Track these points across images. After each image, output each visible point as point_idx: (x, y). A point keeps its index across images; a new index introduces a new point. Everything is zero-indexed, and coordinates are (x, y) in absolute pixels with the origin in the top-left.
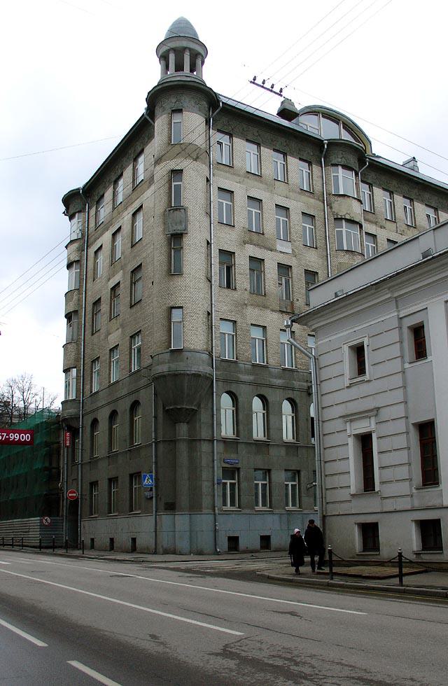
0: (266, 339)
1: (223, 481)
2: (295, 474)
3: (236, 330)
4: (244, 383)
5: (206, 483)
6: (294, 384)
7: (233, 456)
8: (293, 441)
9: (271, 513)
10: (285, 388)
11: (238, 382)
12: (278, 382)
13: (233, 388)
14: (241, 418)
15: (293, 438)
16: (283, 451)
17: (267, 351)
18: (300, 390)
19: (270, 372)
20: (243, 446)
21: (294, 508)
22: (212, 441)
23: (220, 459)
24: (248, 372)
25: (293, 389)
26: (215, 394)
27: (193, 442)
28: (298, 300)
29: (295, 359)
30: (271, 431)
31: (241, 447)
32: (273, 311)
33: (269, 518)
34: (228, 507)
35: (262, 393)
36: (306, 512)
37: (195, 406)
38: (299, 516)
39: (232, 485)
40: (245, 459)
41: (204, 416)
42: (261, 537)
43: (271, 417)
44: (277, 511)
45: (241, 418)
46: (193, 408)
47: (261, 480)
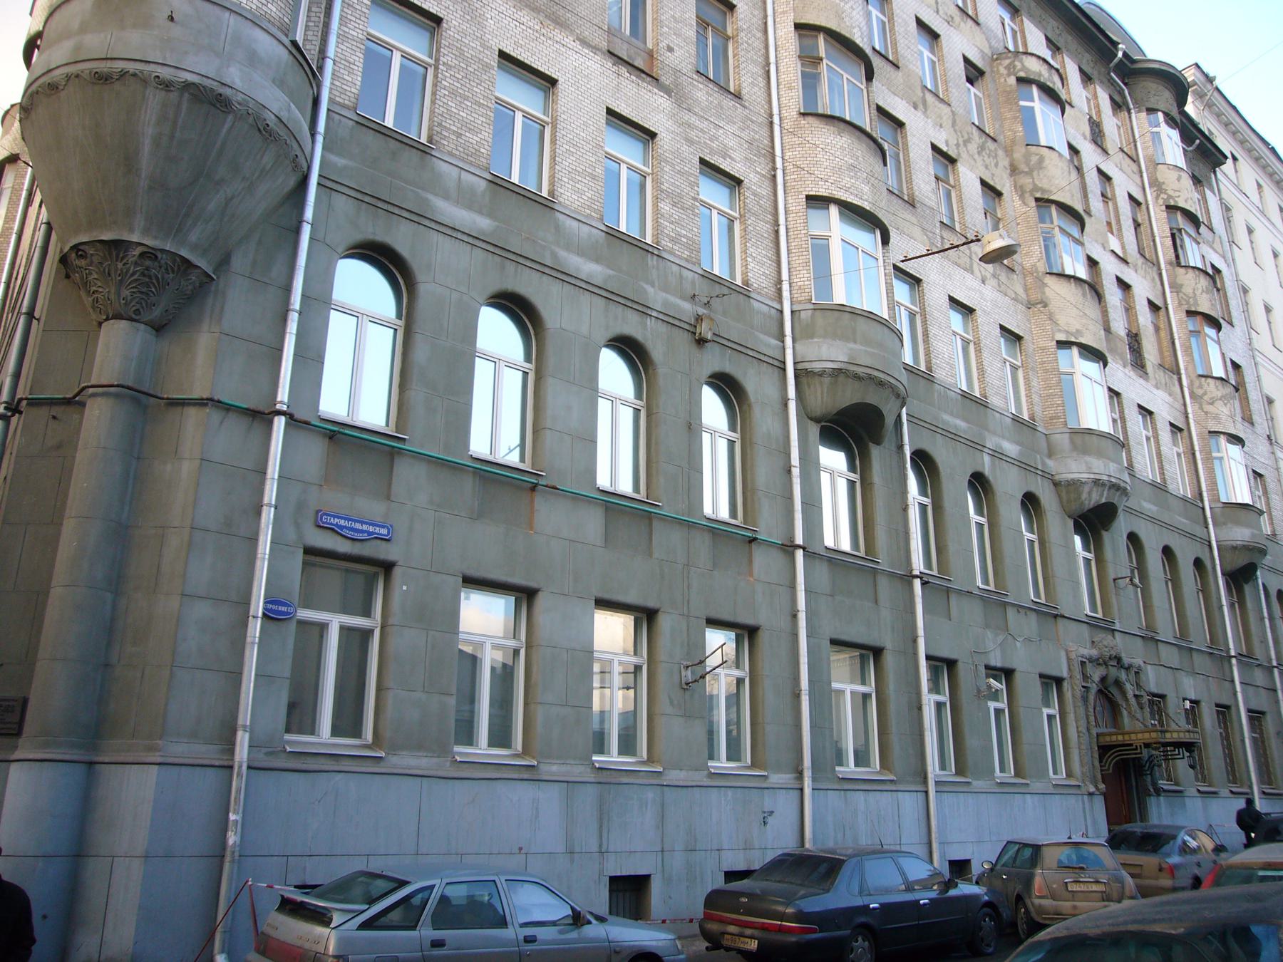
0: (923, 309)
1: (304, 614)
2: (863, 660)
3: (438, 51)
4: (452, 231)
5: (202, 610)
6: (645, 292)
7: (372, 508)
8: (513, 459)
9: (530, 775)
10: (610, 296)
11: (420, 218)
12: (589, 269)
13: (401, 238)
14: (431, 370)
15: (387, 425)
16: (593, 524)
17: (553, 158)
18: (670, 321)
19: (558, 228)
20: (421, 470)
21: (345, 744)
22: (789, 548)
23: (300, 506)
24: (466, 198)
25: (643, 309)
26: (306, 231)
27: (146, 402)
28: (670, 49)
29: (656, 221)
30: (548, 437)
31: (406, 472)
32: (584, 42)
33: (517, 797)
34: (482, 748)
35: (381, 236)
36: (675, 776)
37: (194, 248)
38: (650, 794)
39: (356, 641)
40: (411, 520)
41: (237, 304)
42: (614, 880)
43: (551, 384)
44: (552, 769)
45: (431, 370)
46: (184, 253)
47: (345, 610)
